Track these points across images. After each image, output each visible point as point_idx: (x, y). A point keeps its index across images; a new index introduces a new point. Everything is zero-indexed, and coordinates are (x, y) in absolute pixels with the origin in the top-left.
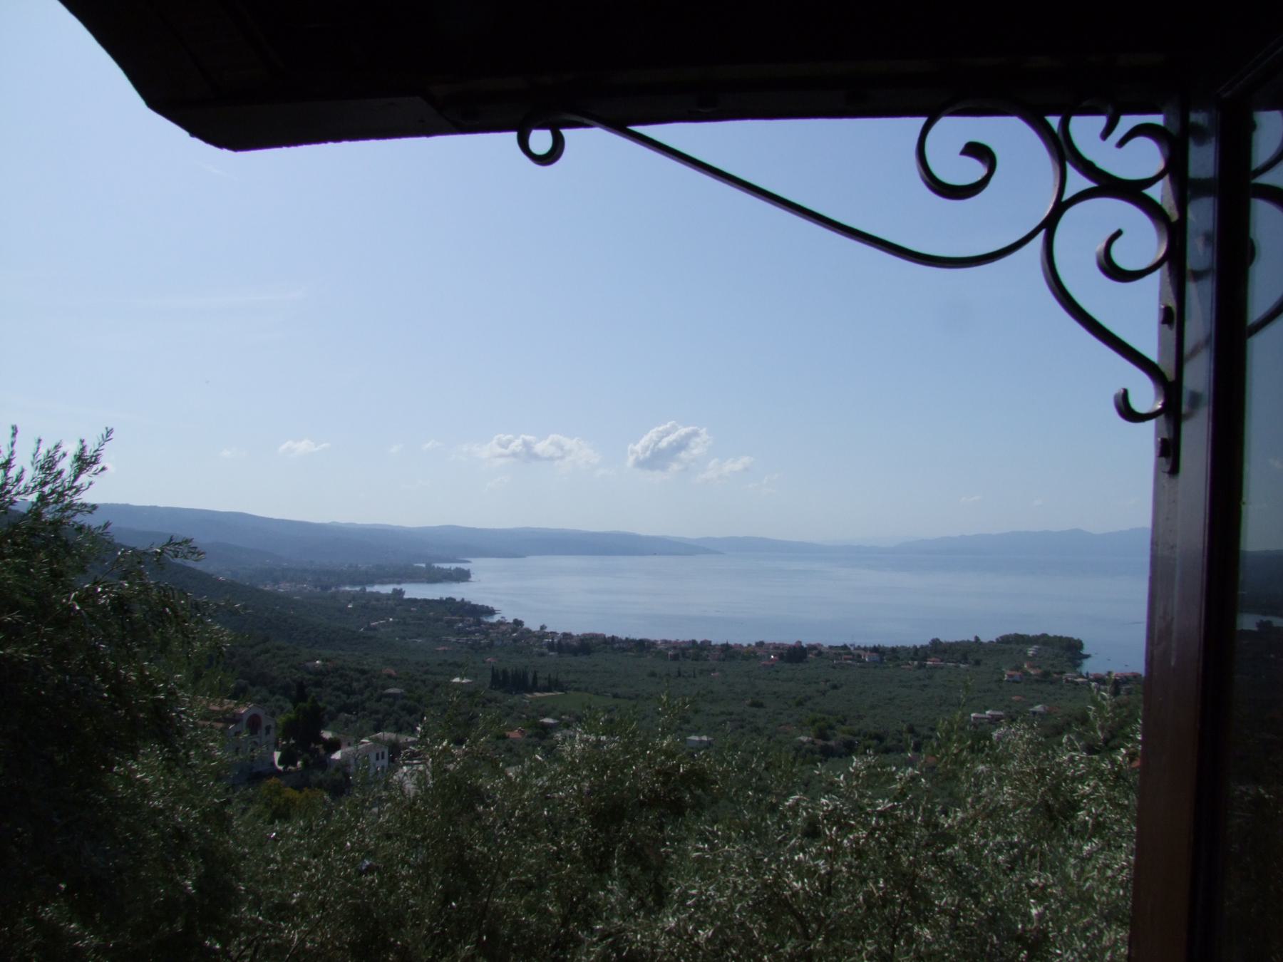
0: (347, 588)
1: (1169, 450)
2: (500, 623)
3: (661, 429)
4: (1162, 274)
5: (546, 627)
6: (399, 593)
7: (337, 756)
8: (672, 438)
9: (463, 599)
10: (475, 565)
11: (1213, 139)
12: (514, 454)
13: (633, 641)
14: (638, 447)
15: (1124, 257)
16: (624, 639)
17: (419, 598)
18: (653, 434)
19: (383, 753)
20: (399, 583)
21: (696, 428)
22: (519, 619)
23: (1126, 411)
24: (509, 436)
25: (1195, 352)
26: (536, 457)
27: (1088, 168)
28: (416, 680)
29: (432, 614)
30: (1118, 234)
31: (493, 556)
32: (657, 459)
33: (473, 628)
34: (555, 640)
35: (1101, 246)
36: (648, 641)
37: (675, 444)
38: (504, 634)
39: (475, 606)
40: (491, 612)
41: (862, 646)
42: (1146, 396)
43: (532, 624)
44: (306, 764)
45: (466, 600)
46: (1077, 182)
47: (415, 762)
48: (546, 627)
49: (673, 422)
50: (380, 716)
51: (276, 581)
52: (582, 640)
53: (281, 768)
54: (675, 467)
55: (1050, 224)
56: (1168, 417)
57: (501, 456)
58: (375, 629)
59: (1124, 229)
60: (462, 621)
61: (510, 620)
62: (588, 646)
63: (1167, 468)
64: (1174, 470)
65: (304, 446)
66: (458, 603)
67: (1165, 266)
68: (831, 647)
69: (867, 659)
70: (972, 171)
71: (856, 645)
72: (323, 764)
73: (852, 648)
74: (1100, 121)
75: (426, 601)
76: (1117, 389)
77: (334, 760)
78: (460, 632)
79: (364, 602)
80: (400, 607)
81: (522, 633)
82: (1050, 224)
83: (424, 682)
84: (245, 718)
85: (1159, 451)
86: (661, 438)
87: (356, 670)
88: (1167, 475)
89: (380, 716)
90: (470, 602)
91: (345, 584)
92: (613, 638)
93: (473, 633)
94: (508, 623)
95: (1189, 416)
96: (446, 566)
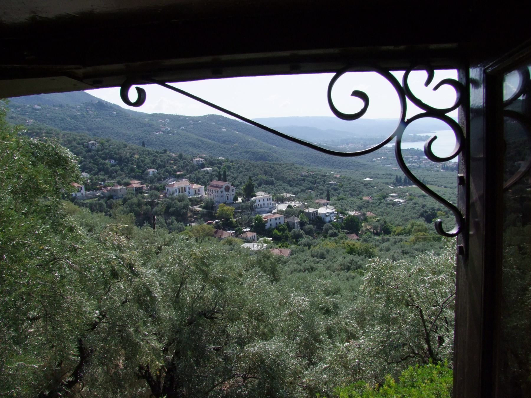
11: (482, 86)
27: (418, 103)
33: (416, 160)
46: (413, 110)
60: (412, 158)
70: (358, 104)
74: (423, 74)
96: (422, 135)
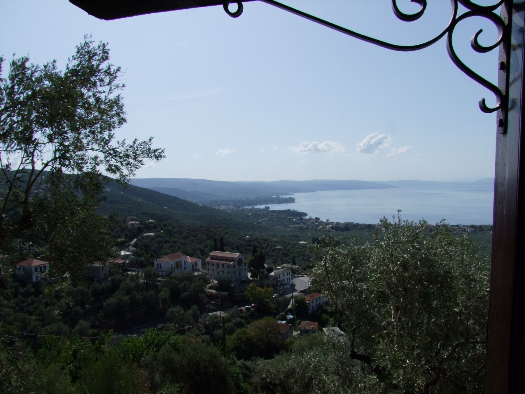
0: (247, 207)
1: (503, 124)
2: (310, 219)
3: (371, 136)
4: (500, 48)
5: (329, 220)
6: (267, 208)
7: (272, 274)
8: (376, 139)
9: (294, 210)
10: (296, 196)
12: (310, 150)
13: (366, 225)
14: (361, 144)
15: (483, 42)
16: (362, 224)
17: (276, 210)
18: (367, 138)
19: (289, 273)
20: (267, 204)
21: (385, 135)
22: (318, 217)
23: (484, 108)
24: (308, 142)
25: (514, 81)
26: (318, 150)
28: (286, 243)
29: (282, 216)
30: (481, 31)
31: (305, 192)
32: (369, 149)
33: (299, 221)
34: (334, 225)
35: (473, 37)
36: (372, 225)
37: (377, 142)
38: (312, 223)
39: (299, 212)
40: (305, 215)
41: (466, 225)
42: (493, 101)
43: (323, 219)
44: (261, 277)
45: (295, 210)
46: (462, 10)
47: (300, 276)
48: (329, 220)
49: (376, 133)
50: (275, 258)
51: (219, 205)
52: (346, 225)
53: (251, 279)
54: (377, 152)
55: (450, 30)
56: (502, 110)
57: (305, 151)
58: (260, 223)
59: (483, 29)
60: (295, 219)
61: (314, 218)
62: (348, 227)
63: (502, 132)
64: (505, 132)
65: (226, 151)
66: (292, 211)
67: (502, 43)
68: (451, 226)
69: (469, 231)
71: (463, 225)
72: (267, 277)
73: (461, 226)
75: (279, 211)
76: (481, 99)
77: (271, 275)
78: (294, 223)
79: (254, 212)
80: (269, 214)
81: (319, 223)
82: (450, 30)
83: (289, 243)
84: (237, 260)
85: (498, 124)
86: (371, 140)
87: (263, 239)
88: (502, 135)
89: (275, 258)
90: (297, 211)
91: (246, 205)
92: (358, 224)
93: (300, 223)
94: (313, 219)
95: (512, 108)
96: (284, 197)
